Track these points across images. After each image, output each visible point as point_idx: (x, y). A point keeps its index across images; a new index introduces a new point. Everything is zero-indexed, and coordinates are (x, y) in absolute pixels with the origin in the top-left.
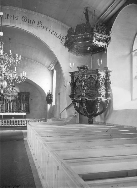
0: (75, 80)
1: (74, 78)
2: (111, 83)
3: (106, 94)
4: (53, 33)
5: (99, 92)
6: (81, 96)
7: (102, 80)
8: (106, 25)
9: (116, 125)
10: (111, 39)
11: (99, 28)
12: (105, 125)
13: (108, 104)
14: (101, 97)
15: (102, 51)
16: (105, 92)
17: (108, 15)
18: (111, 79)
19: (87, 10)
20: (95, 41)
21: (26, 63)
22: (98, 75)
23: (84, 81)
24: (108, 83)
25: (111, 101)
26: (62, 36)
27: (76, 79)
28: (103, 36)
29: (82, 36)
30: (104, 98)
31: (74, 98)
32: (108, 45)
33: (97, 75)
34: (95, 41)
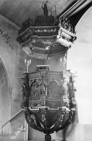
1: (28, 80)
2: (75, 90)
3: (70, 104)
8: (73, 20)
10: (77, 38)
15: (63, 50)
18: (76, 85)
19: (45, 5)
20: (60, 38)
22: (63, 79)
24: (73, 90)
27: (32, 83)
30: (68, 108)
32: (46, 52)
33: (61, 79)
34: (60, 38)
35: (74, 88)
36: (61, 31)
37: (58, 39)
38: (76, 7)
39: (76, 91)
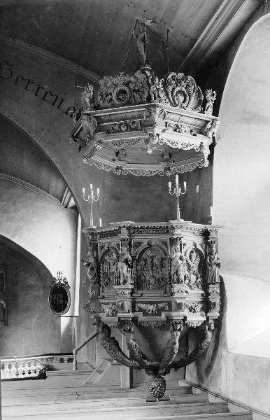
0: (100, 255)
4: (48, 98)
5: (176, 295)
7: (190, 257)
9: (240, 405)
14: (186, 312)
16: (202, 295)
17: (214, 40)
28: (190, 114)
35: (216, 258)
36: (163, 113)
37: (158, 135)
38: (221, 23)
39: (219, 267)
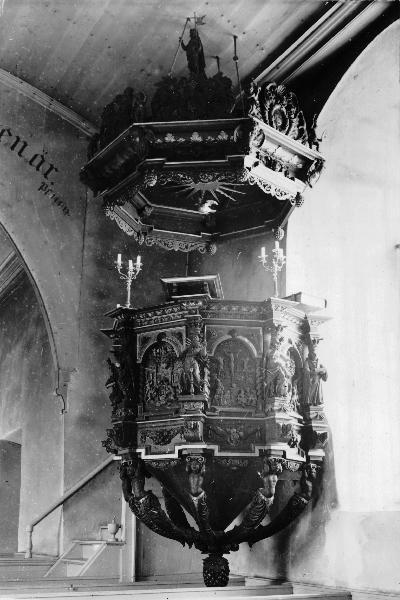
5: (278, 415)
6: (177, 438)
10: (325, 164)
11: (272, 106)
12: (243, 587)
13: (310, 484)
18: (324, 355)
20: (256, 164)
21: (30, 58)
23: (198, 357)
25: (323, 467)
26: (49, 160)
27: (149, 351)
29: (189, 131)
30: (295, 450)
31: (136, 447)
33: (265, 331)
34: (256, 164)
